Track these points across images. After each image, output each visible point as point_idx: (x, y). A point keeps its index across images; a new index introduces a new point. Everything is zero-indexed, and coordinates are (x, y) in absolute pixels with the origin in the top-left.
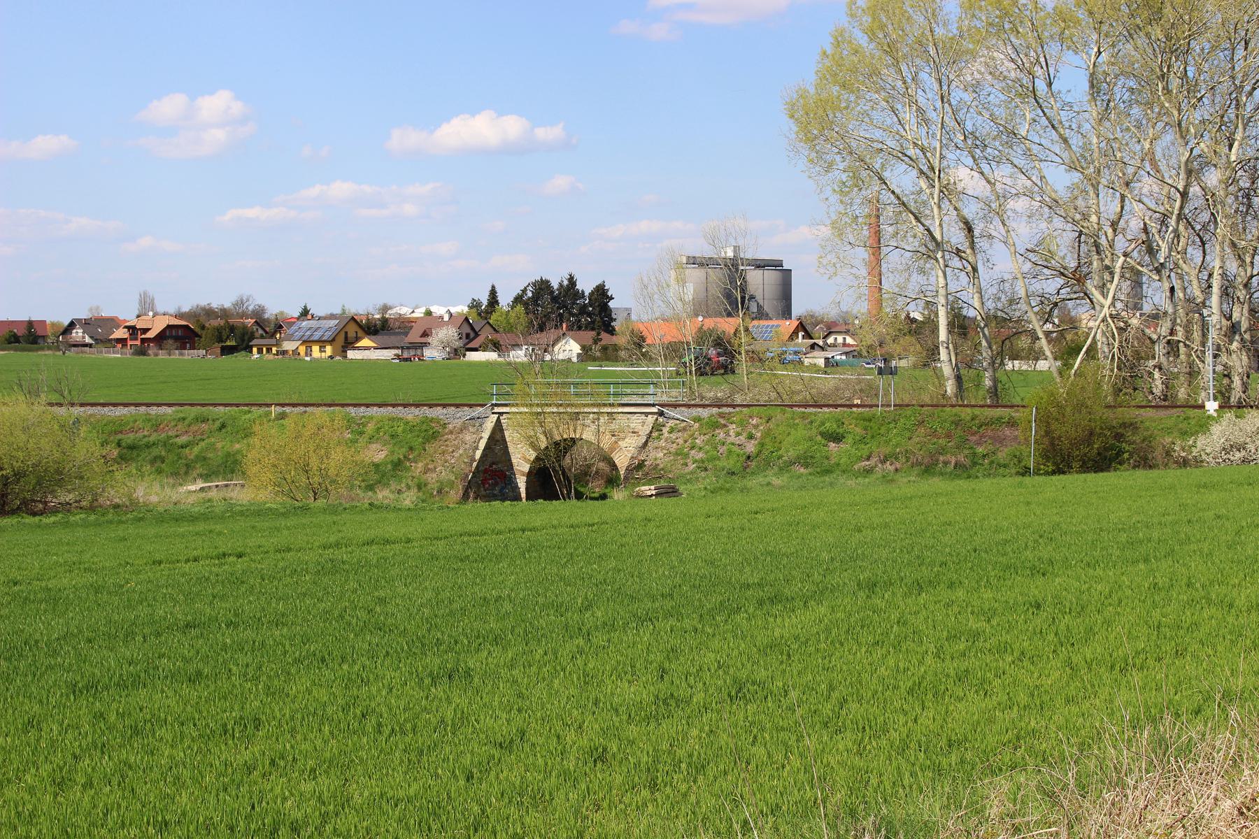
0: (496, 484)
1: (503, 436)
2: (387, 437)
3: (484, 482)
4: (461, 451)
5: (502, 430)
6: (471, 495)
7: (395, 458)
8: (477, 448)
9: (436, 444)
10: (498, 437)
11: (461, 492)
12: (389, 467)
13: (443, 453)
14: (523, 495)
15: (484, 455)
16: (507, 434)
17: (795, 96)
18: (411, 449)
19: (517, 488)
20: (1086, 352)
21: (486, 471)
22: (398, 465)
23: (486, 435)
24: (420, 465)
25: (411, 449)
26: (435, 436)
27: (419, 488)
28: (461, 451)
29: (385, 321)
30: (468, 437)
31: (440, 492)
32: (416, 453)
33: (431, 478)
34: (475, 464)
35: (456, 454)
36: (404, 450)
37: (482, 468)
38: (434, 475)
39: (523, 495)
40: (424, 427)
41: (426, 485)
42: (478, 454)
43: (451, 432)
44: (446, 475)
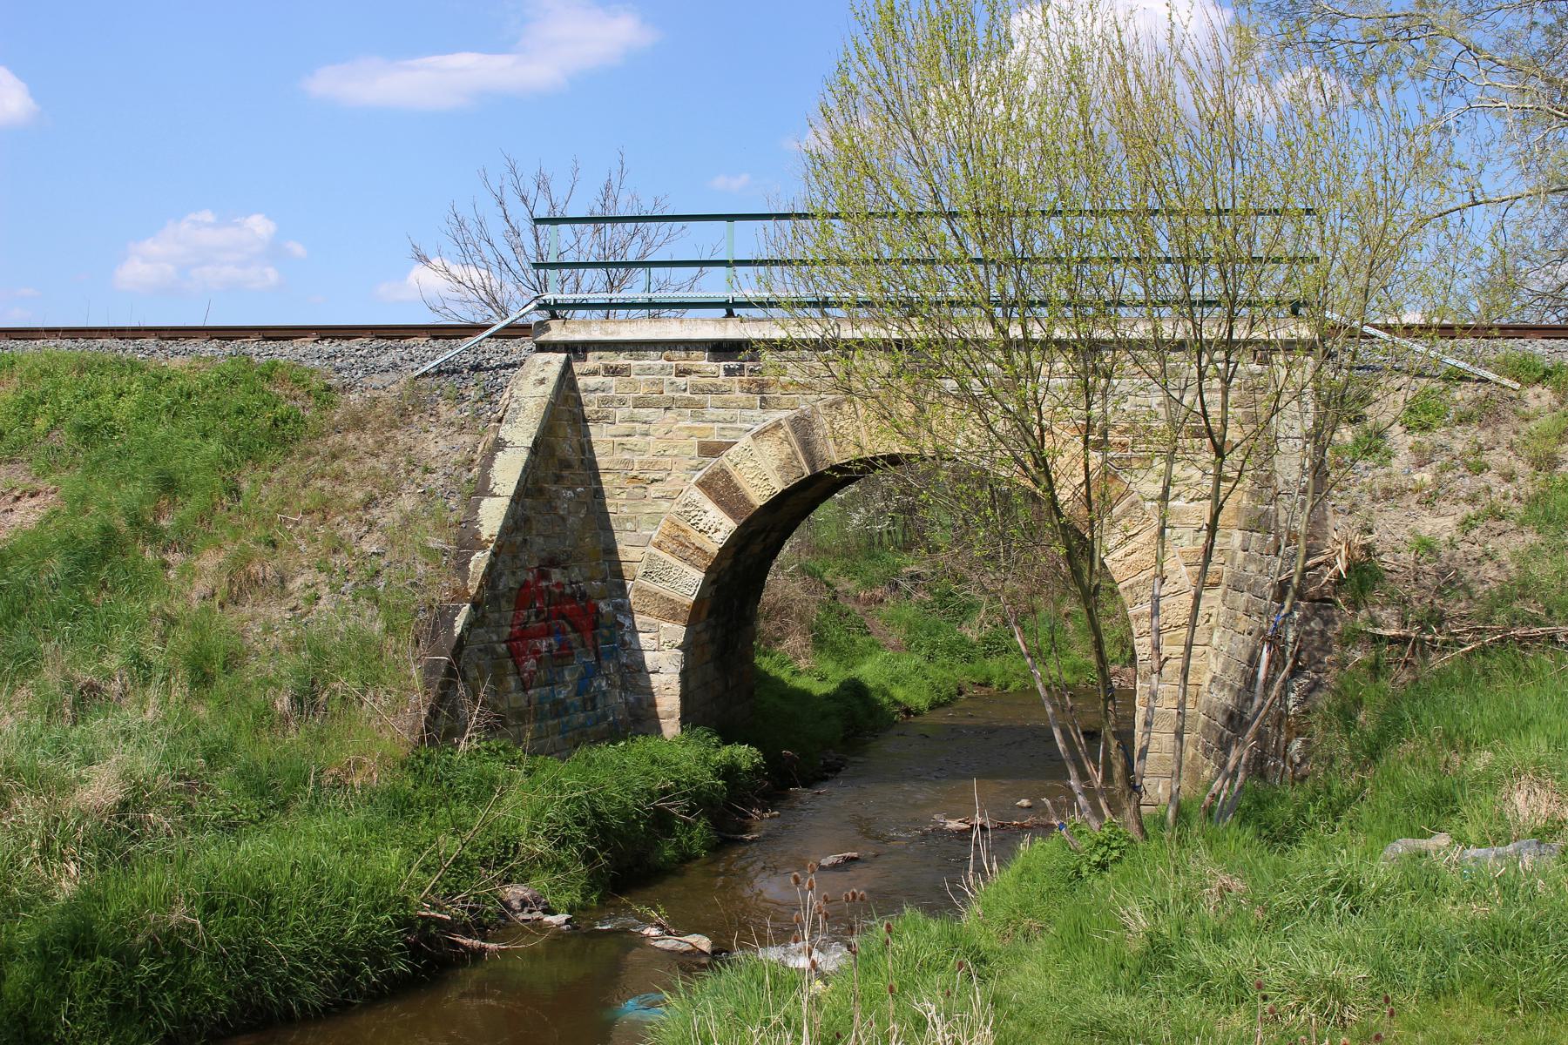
0: (562, 656)
1: (586, 448)
2: (64, 438)
3: (518, 645)
4: (408, 502)
5: (580, 422)
6: (474, 716)
7: (88, 526)
8: (482, 489)
9: (288, 470)
10: (566, 449)
11: (419, 700)
12: (56, 565)
13: (323, 509)
14: (668, 700)
15: (516, 522)
16: (598, 433)
17: (1250, 831)
18: (169, 485)
19: (635, 672)
20: (1109, 807)
21: (523, 597)
22: (98, 558)
23: (521, 434)
24: (210, 560)
25: (169, 485)
26: (283, 435)
27: (202, 679)
28: (408, 502)
29: (687, 349)
30: (438, 444)
31: (306, 700)
32: (193, 506)
33: (263, 624)
34: (479, 562)
35: (387, 517)
36: (134, 490)
37: (507, 582)
38: (278, 612)
39: (668, 700)
40: (238, 397)
41: (232, 662)
42: (492, 516)
43: (358, 423)
44: (335, 614)
